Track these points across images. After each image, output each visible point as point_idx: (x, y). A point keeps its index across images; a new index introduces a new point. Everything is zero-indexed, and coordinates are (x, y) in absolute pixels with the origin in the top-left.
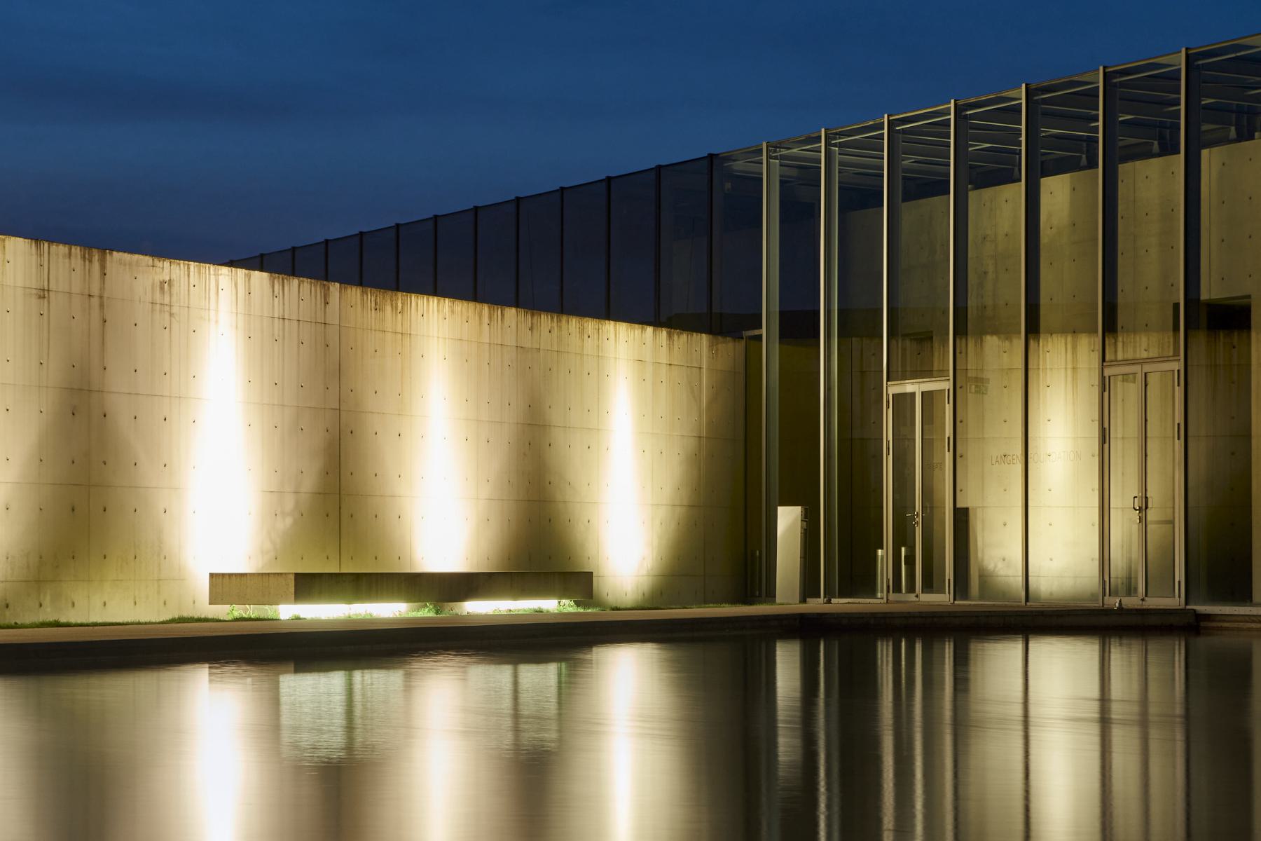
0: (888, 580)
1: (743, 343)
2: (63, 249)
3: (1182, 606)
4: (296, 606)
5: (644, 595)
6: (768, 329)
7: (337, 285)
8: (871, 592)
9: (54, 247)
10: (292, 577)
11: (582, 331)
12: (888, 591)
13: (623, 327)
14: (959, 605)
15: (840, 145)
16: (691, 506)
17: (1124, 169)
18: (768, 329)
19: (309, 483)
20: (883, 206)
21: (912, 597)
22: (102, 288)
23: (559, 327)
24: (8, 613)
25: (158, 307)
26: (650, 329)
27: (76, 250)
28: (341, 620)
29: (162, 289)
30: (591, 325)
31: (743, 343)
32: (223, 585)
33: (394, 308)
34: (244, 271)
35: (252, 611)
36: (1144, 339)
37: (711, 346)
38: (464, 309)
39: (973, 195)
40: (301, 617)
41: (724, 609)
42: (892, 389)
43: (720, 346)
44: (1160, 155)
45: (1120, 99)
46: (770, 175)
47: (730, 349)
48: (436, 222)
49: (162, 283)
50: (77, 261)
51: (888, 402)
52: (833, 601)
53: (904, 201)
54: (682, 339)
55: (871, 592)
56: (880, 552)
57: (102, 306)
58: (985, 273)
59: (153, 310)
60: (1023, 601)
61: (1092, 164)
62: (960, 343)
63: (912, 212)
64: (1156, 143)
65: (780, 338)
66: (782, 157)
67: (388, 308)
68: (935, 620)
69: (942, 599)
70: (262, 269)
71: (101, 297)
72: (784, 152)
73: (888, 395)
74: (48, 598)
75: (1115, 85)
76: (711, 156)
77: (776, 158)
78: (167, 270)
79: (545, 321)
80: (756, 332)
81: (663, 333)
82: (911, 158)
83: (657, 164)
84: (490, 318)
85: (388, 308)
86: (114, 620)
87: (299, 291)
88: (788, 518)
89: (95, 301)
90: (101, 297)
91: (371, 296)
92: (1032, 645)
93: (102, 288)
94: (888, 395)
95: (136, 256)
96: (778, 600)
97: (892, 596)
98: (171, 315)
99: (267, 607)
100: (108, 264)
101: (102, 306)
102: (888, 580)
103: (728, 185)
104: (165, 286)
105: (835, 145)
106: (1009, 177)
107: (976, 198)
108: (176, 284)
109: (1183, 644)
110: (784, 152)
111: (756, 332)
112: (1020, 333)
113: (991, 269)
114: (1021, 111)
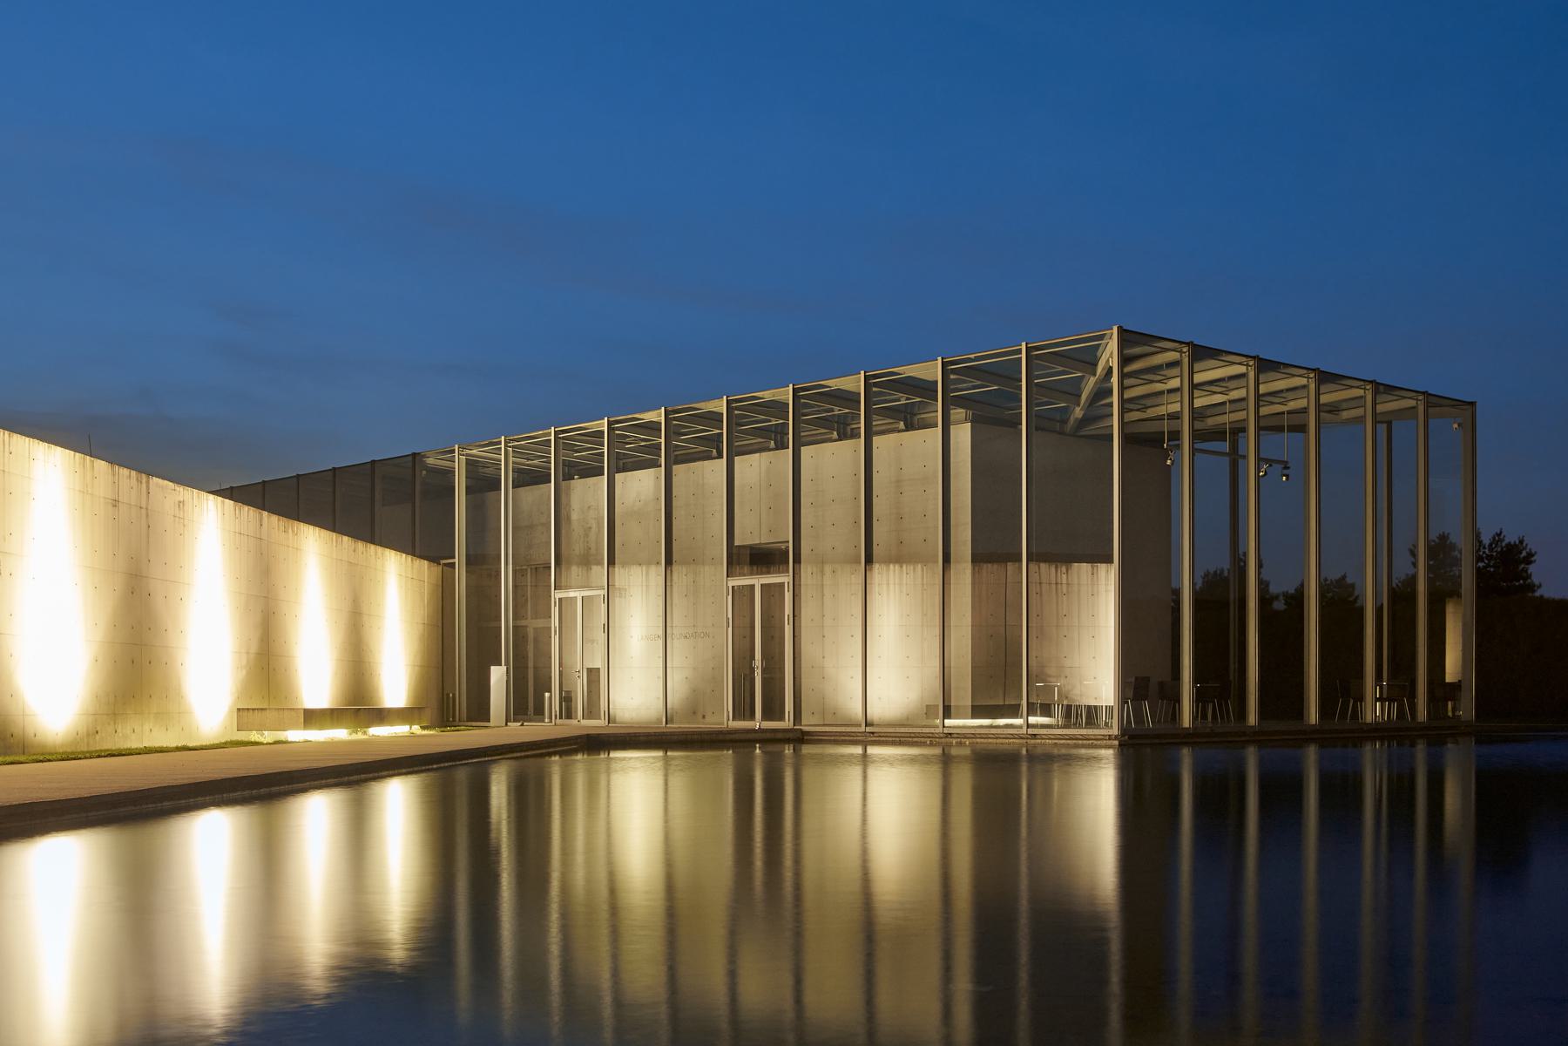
2: (125, 472)
4: (306, 731)
6: (460, 558)
8: (782, 718)
12: (556, 718)
13: (393, 552)
14: (670, 728)
15: (513, 447)
16: (421, 666)
17: (806, 451)
18: (460, 558)
19: (254, 649)
20: (501, 490)
21: (574, 722)
25: (177, 519)
27: (133, 473)
28: (319, 742)
29: (179, 506)
30: (380, 549)
33: (293, 531)
34: (221, 498)
36: (684, 569)
37: (429, 568)
38: (325, 534)
39: (618, 477)
40: (290, 740)
42: (557, 595)
50: (134, 482)
51: (555, 603)
52: (525, 724)
55: (782, 718)
56: (547, 695)
57: (147, 516)
58: (590, 528)
59: (175, 521)
60: (664, 723)
61: (720, 456)
64: (715, 451)
66: (467, 455)
67: (290, 531)
68: (664, 737)
69: (787, 723)
73: (555, 599)
74: (120, 727)
76: (414, 455)
77: (463, 455)
79: (360, 545)
83: (372, 459)
84: (337, 541)
85: (290, 531)
87: (248, 512)
89: (144, 511)
90: (147, 509)
94: (555, 599)
95: (166, 482)
96: (492, 724)
98: (184, 526)
100: (151, 486)
101: (147, 516)
102: (556, 712)
104: (181, 503)
105: (510, 447)
108: (186, 503)
113: (594, 526)
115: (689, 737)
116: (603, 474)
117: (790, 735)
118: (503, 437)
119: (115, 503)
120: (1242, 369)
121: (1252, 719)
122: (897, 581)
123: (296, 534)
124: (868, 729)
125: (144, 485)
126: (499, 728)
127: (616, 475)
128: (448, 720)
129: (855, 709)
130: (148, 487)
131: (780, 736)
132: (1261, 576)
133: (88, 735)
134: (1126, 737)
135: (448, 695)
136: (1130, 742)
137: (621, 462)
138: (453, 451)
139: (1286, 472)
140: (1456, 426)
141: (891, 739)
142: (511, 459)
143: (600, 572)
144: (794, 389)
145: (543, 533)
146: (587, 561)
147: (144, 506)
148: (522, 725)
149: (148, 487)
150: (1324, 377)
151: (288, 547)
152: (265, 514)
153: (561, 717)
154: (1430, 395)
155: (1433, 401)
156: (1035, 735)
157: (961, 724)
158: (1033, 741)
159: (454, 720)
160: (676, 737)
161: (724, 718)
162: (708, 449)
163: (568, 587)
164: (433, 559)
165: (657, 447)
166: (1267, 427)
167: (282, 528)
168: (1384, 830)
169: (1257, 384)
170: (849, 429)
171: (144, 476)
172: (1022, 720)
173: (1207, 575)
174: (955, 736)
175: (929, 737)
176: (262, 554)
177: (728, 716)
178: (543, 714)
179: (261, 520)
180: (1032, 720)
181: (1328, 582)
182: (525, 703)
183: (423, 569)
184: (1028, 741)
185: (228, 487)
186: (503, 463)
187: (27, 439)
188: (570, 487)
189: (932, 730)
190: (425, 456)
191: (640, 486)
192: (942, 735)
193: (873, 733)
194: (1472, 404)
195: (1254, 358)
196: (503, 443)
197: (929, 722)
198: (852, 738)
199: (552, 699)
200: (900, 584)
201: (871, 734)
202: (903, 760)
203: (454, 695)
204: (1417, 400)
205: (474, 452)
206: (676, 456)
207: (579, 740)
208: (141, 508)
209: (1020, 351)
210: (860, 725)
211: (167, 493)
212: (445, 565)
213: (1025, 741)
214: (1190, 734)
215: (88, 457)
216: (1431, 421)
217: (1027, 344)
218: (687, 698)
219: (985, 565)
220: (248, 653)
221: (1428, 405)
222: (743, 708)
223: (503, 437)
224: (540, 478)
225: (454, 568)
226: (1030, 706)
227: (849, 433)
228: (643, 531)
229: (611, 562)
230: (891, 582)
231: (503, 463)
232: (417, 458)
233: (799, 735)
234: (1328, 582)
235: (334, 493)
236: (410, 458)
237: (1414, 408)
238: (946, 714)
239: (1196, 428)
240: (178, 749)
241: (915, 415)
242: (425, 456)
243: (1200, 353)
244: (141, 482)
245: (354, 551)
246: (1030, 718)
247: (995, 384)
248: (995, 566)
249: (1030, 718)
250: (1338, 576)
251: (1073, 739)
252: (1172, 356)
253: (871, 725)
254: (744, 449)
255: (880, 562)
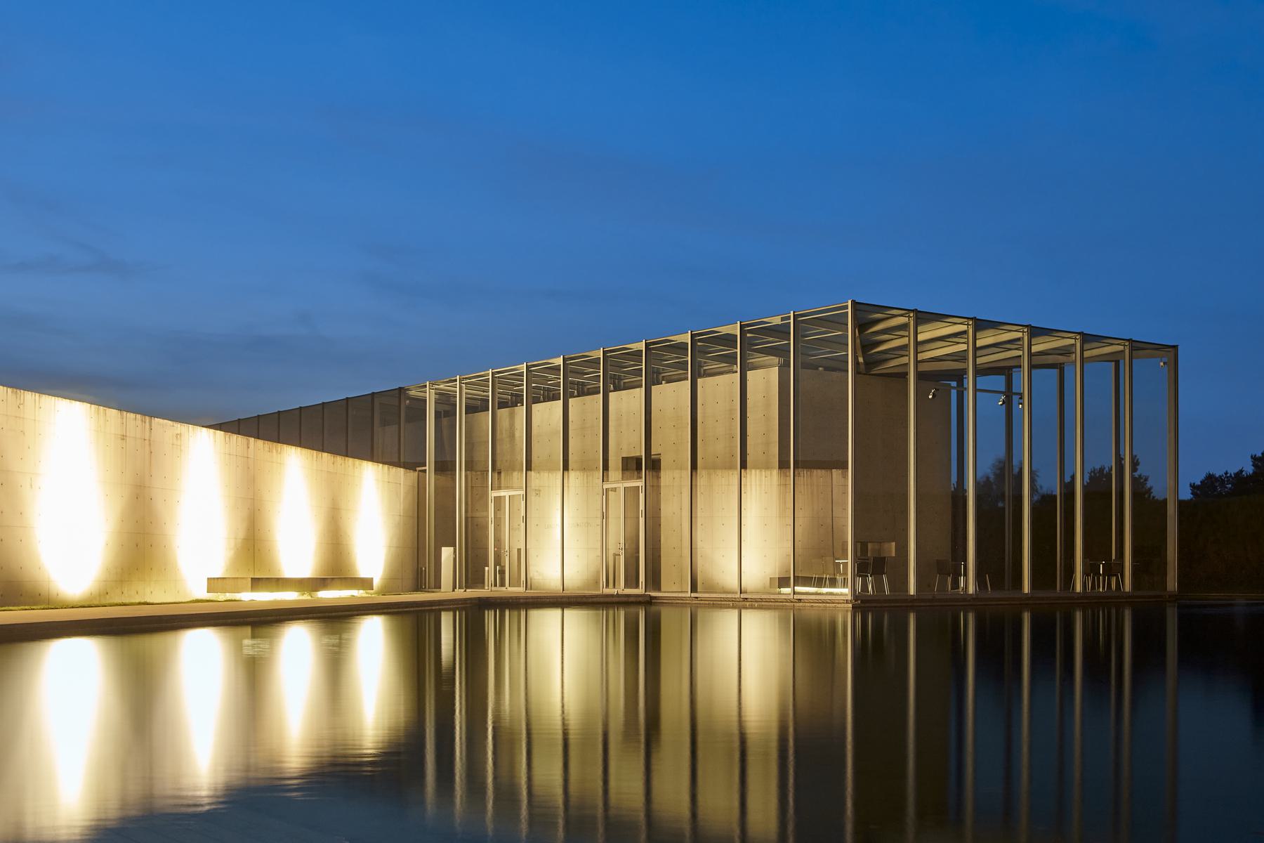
0: (603, 582)
1: (417, 473)
2: (132, 416)
3: (644, 592)
5: (91, 594)
7: (253, 439)
9: (128, 414)
10: (250, 579)
11: (354, 465)
15: (466, 383)
19: (241, 534)
21: (503, 589)
22: (150, 436)
23: (345, 463)
24: (108, 597)
25: (175, 446)
26: (381, 465)
27: (139, 416)
29: (177, 437)
30: (357, 462)
31: (417, 473)
32: (213, 584)
33: (277, 451)
34: (213, 430)
35: (229, 596)
41: (433, 594)
42: (493, 494)
43: (408, 474)
44: (578, 396)
45: (699, 351)
46: (430, 397)
47: (413, 475)
48: (279, 415)
49: (177, 434)
50: (139, 422)
52: (468, 590)
53: (498, 409)
54: (394, 470)
55: (637, 587)
56: (487, 568)
57: (150, 444)
62: (529, 472)
63: (503, 413)
65: (435, 471)
66: (436, 389)
67: (274, 451)
70: (221, 430)
71: (150, 440)
72: (437, 387)
74: (126, 589)
75: (608, 356)
76: (400, 388)
78: (179, 429)
79: (339, 459)
80: (423, 468)
81: (386, 467)
82: (549, 385)
84: (317, 457)
85: (274, 451)
86: (165, 601)
88: (447, 553)
89: (147, 442)
90: (150, 440)
91: (268, 444)
92: (565, 611)
93: (150, 436)
95: (166, 421)
96: (442, 590)
97: (493, 588)
99: (236, 594)
100: (153, 425)
101: (150, 444)
102: (603, 582)
103: (408, 402)
104: (178, 436)
106: (556, 398)
107: (536, 408)
109: (644, 609)
110: (437, 387)
111: (423, 468)
112: (560, 470)
114: (560, 370)
115: (559, 600)
116: (488, 410)
117: (641, 599)
118: (458, 376)
119: (123, 437)
120: (964, 328)
121: (1026, 588)
122: (758, 483)
123: (280, 453)
124: (742, 596)
125: (147, 424)
126: (447, 589)
127: (653, 387)
128: (421, 587)
129: (732, 583)
130: (151, 425)
131: (632, 599)
132: (1141, 470)
133: (100, 595)
134: (859, 602)
135: (421, 568)
136: (863, 605)
137: (552, 393)
138: (426, 386)
139: (1021, 401)
140: (1162, 364)
141: (707, 602)
142: (464, 391)
143: (518, 477)
144: (646, 343)
145: (341, 465)
146: (512, 468)
147: (147, 438)
148: (465, 591)
149: (151, 425)
150: (1035, 332)
151: (273, 462)
152: (252, 440)
153: (496, 585)
154: (1134, 341)
155: (1136, 346)
156: (800, 600)
157: (804, 591)
158: (798, 604)
159: (425, 588)
160: (548, 600)
161: (621, 589)
162: (551, 396)
163: (499, 488)
164: (409, 466)
165: (731, 357)
166: (980, 371)
167: (267, 449)
168: (11, 608)
169: (975, 339)
170: (622, 382)
171: (147, 418)
172: (790, 589)
173: (1093, 471)
174: (750, 600)
175: (733, 601)
176: (248, 468)
177: (603, 585)
178: (484, 583)
179: (248, 444)
180: (798, 589)
181: (1228, 475)
182: (472, 571)
183: (401, 476)
184: (795, 604)
185: (256, 415)
186: (458, 393)
187: (53, 398)
188: (514, 412)
189: (733, 596)
190: (408, 390)
191: (548, 414)
192: (741, 600)
193: (697, 598)
194: (1175, 347)
195: (972, 319)
196: (491, 375)
197: (772, 590)
198: (682, 601)
199: (489, 571)
200: (760, 485)
201: (743, 602)
202: (844, 621)
203: (425, 568)
204: (1124, 345)
205: (442, 386)
206: (624, 383)
207: (469, 602)
208: (145, 440)
209: (846, 307)
210: (736, 593)
211: (165, 428)
212: (420, 471)
213: (792, 604)
214: (914, 600)
215: (102, 407)
216: (1134, 360)
217: (794, 312)
218: (279, 570)
219: (815, 471)
220: (236, 539)
221: (1132, 350)
222: (632, 580)
223: (458, 376)
224: (516, 401)
225: (426, 473)
226: (796, 578)
227: (702, 372)
228: (585, 442)
229: (529, 468)
230: (753, 483)
231: (458, 393)
232: (402, 391)
233: (648, 599)
234: (1228, 475)
235: (258, 433)
236: (397, 391)
237: (1122, 351)
238: (796, 583)
239: (919, 370)
240: (140, 604)
241: (661, 373)
242: (408, 390)
243: (923, 317)
244: (145, 422)
245: (333, 463)
246: (796, 588)
247: (840, 331)
248: (823, 471)
249: (796, 588)
250: (1236, 470)
251: (824, 603)
252: (902, 320)
253: (746, 592)
254: (635, 384)
255: (756, 467)
